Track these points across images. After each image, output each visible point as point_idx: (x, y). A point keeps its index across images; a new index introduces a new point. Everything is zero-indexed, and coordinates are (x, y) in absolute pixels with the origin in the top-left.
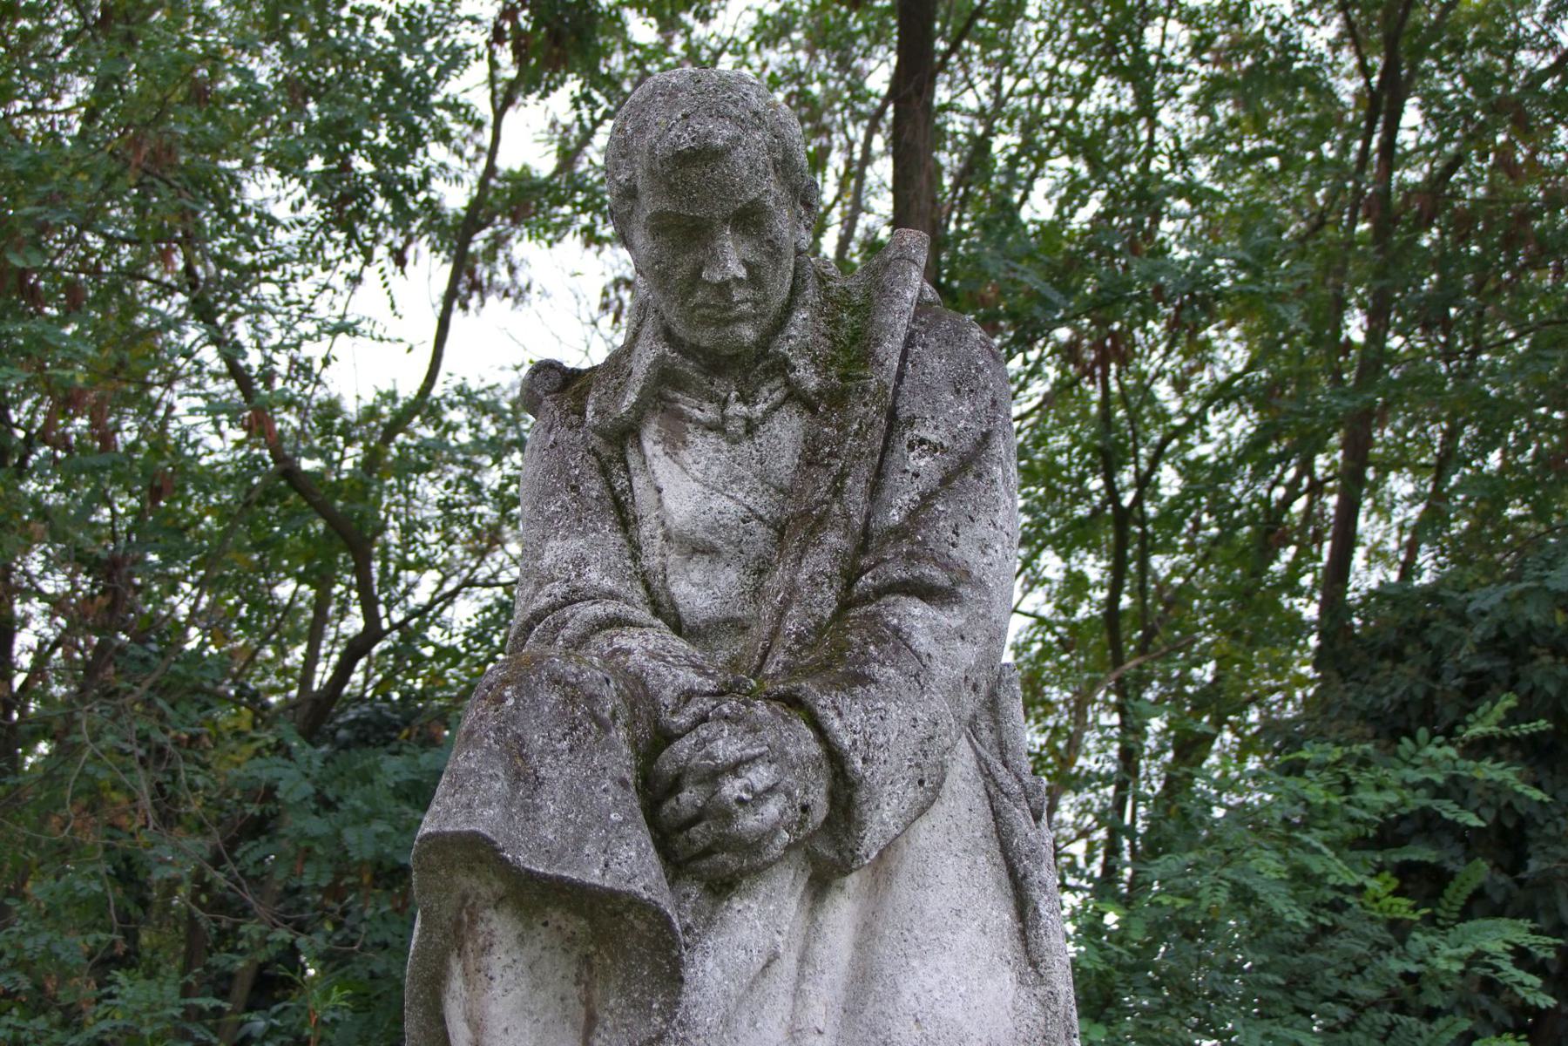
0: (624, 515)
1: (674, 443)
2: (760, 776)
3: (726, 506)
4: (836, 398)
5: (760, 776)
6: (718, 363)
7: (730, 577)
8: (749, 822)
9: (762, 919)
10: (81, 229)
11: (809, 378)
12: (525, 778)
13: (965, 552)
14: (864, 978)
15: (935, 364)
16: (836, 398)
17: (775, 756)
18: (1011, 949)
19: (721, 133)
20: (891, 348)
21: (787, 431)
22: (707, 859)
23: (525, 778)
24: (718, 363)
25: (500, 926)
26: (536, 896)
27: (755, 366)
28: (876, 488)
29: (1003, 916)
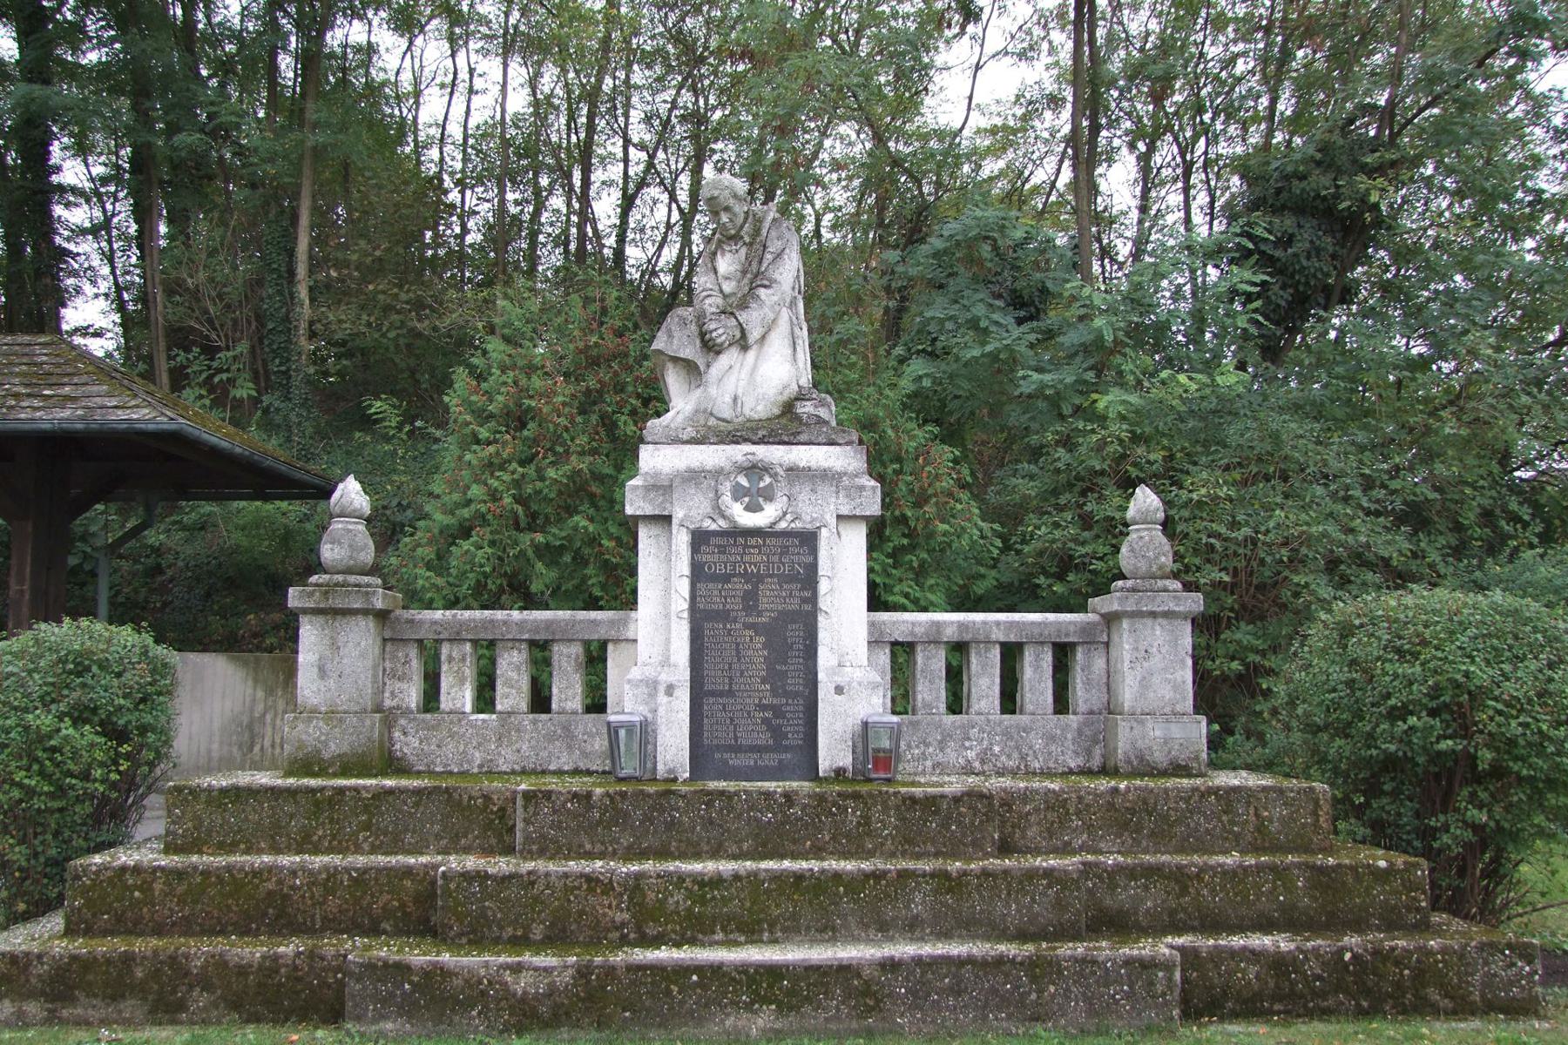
0: (716, 272)
1: (723, 255)
2: (720, 331)
3: (732, 269)
4: (751, 244)
5: (720, 331)
6: (731, 238)
7: (734, 283)
8: (719, 341)
9: (724, 360)
10: (412, 424)
11: (747, 239)
12: (670, 336)
13: (776, 276)
14: (755, 368)
15: (773, 233)
16: (751, 244)
17: (725, 327)
18: (790, 358)
19: (716, 193)
20: (764, 232)
21: (744, 251)
22: (711, 348)
23: (670, 336)
24: (731, 238)
25: (670, 365)
26: (675, 360)
27: (735, 238)
28: (760, 262)
29: (790, 351)
